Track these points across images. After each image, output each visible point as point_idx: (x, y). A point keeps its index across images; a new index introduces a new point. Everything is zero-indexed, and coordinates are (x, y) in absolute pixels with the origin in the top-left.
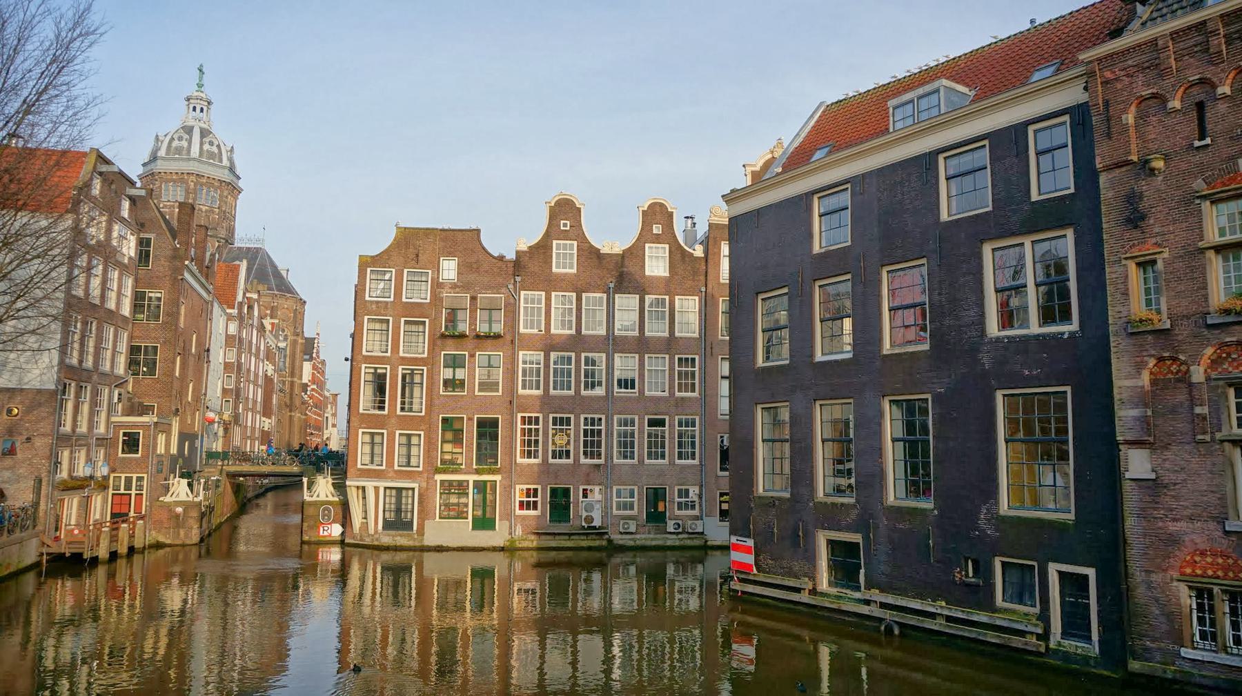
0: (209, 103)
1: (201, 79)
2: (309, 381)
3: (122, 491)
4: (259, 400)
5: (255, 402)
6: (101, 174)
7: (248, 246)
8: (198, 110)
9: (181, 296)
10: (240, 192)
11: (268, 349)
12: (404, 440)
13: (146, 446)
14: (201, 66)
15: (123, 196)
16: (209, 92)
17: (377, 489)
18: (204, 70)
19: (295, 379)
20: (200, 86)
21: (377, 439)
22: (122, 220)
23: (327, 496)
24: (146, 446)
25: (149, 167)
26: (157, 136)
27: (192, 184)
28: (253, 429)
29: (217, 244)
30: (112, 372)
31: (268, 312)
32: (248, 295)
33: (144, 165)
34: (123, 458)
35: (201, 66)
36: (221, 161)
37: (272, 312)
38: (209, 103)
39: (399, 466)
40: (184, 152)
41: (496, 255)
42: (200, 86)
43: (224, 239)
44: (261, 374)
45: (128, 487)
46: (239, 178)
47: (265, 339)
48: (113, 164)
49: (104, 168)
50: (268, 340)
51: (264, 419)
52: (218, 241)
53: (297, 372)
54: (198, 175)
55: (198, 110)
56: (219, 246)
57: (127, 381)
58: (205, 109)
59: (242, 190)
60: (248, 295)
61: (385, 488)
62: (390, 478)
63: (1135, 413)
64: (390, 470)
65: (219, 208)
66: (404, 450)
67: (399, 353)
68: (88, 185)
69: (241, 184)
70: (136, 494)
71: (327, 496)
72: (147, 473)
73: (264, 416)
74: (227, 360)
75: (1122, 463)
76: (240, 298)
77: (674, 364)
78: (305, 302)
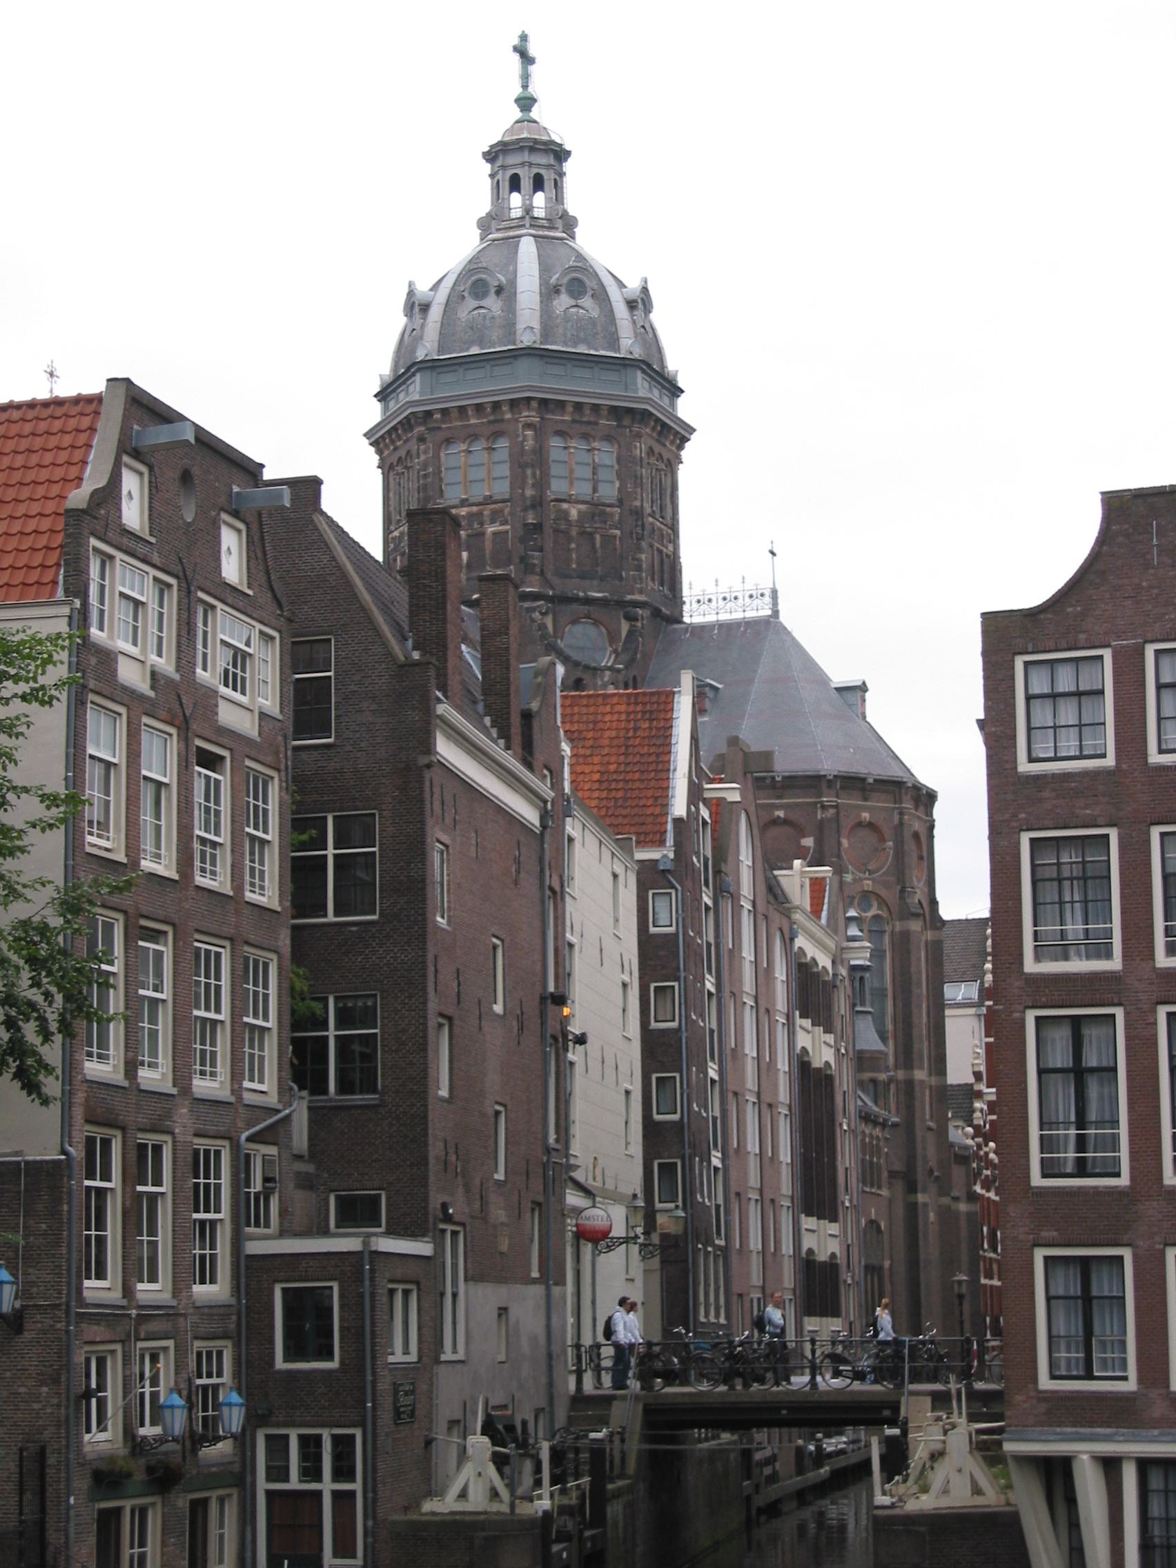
0: (561, 154)
1: (525, 79)
2: (978, 1076)
3: (294, 1483)
4: (785, 1156)
5: (767, 1161)
6: (137, 454)
7: (724, 617)
8: (526, 183)
9: (430, 822)
10: (685, 440)
11: (804, 974)
12: (1068, 1284)
13: (354, 1333)
14: (524, 38)
15: (224, 516)
17: (1110, 1466)
18: (532, 51)
19: (920, 1075)
20: (526, 103)
21: (1101, 1286)
22: (227, 593)
23: (977, 1491)
24: (354, 1333)
25: (393, 406)
27: (529, 433)
28: (769, 1257)
29: (625, 627)
30: (237, 1091)
31: (808, 842)
32: (713, 790)
33: (383, 395)
34: (289, 1372)
35: (524, 38)
36: (614, 342)
37: (819, 842)
38: (561, 154)
39: (1053, 1377)
40: (495, 335)
41: (377, 457)
42: (526, 103)
43: (642, 605)
44: (783, 1064)
45: (312, 1471)
46: (676, 391)
47: (789, 940)
48: (182, 418)
49: (161, 435)
50: (800, 942)
51: (808, 1222)
52: (631, 618)
53: (923, 1047)
54: (544, 402)
55: (526, 183)
56: (631, 633)
57: (288, 1117)
58: (548, 176)
59: (692, 430)
60: (713, 790)
61: (1144, 1465)
62: (1155, 1423)
63: (819, 812)
64: (1154, 1394)
65: (620, 503)
66: (1069, 1325)
67: (1151, 956)
68: (110, 494)
69: (685, 409)
70: (336, 1494)
71: (977, 1491)
72: (362, 1424)
73: (809, 1214)
74: (654, 1025)
75: (48, 1495)
76: (679, 806)
77: (243, 854)
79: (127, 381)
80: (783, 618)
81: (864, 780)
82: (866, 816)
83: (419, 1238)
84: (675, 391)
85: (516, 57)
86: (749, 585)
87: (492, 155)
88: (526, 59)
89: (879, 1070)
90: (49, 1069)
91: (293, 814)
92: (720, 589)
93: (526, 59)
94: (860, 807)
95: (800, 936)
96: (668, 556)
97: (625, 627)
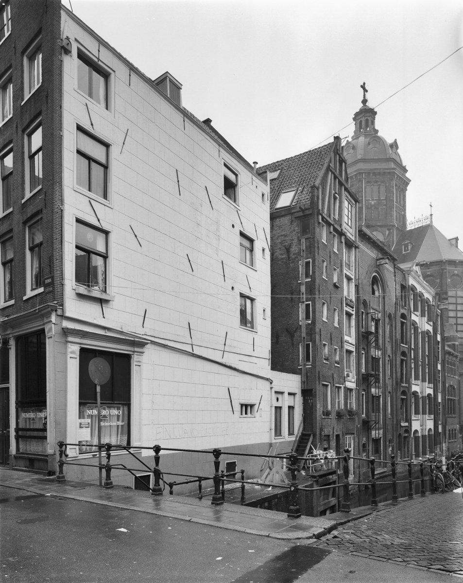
18: (367, 87)
29: (387, 232)
35: (364, 84)
42: (365, 101)
52: (389, 230)
79: (225, 194)
80: (434, 224)
81: (455, 261)
82: (456, 272)
83: (302, 425)
84: (406, 171)
85: (367, 88)
86: (424, 216)
88: (365, 91)
89: (455, 341)
90: (394, 169)
91: (141, 452)
92: (416, 219)
93: (365, 91)
94: (454, 270)
95: (413, 390)
96: (402, 215)
97: (387, 232)
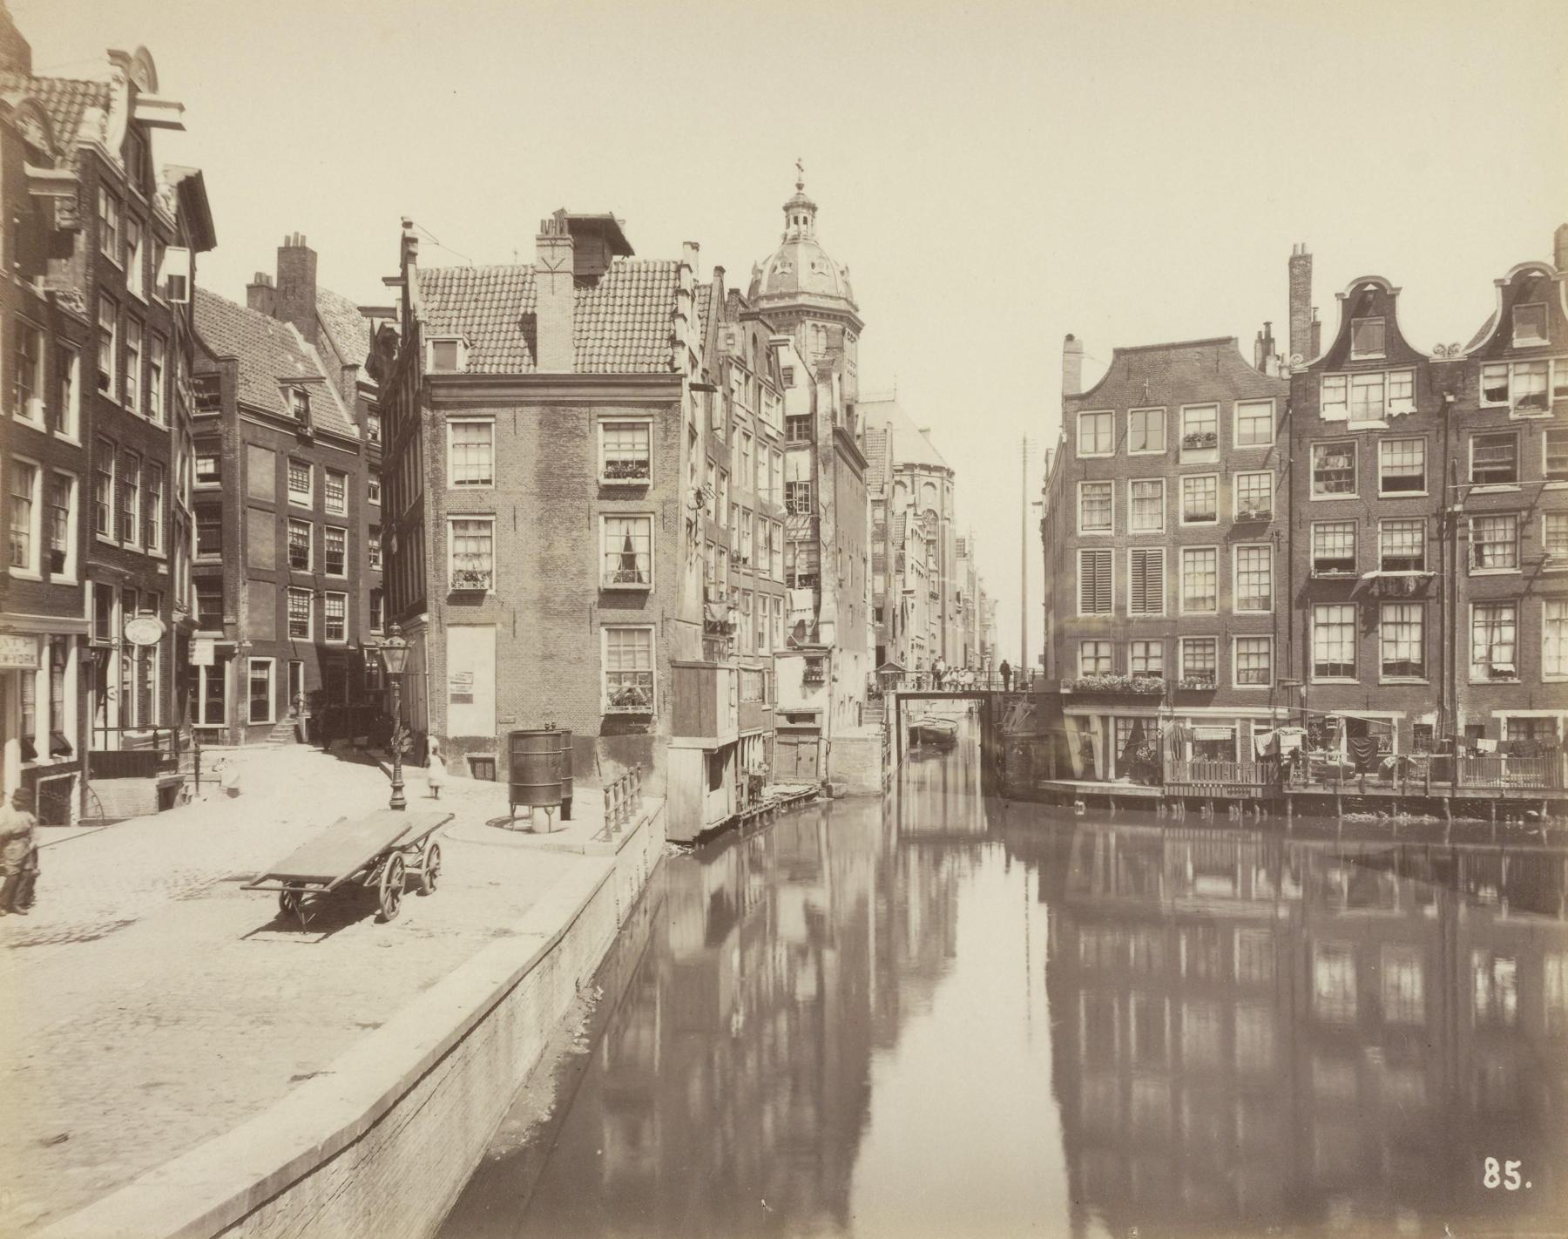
16: (810, 195)
18: (803, 167)
26: (755, 266)
46: (857, 310)
55: (801, 220)
78: (953, 473)
87: (786, 209)
